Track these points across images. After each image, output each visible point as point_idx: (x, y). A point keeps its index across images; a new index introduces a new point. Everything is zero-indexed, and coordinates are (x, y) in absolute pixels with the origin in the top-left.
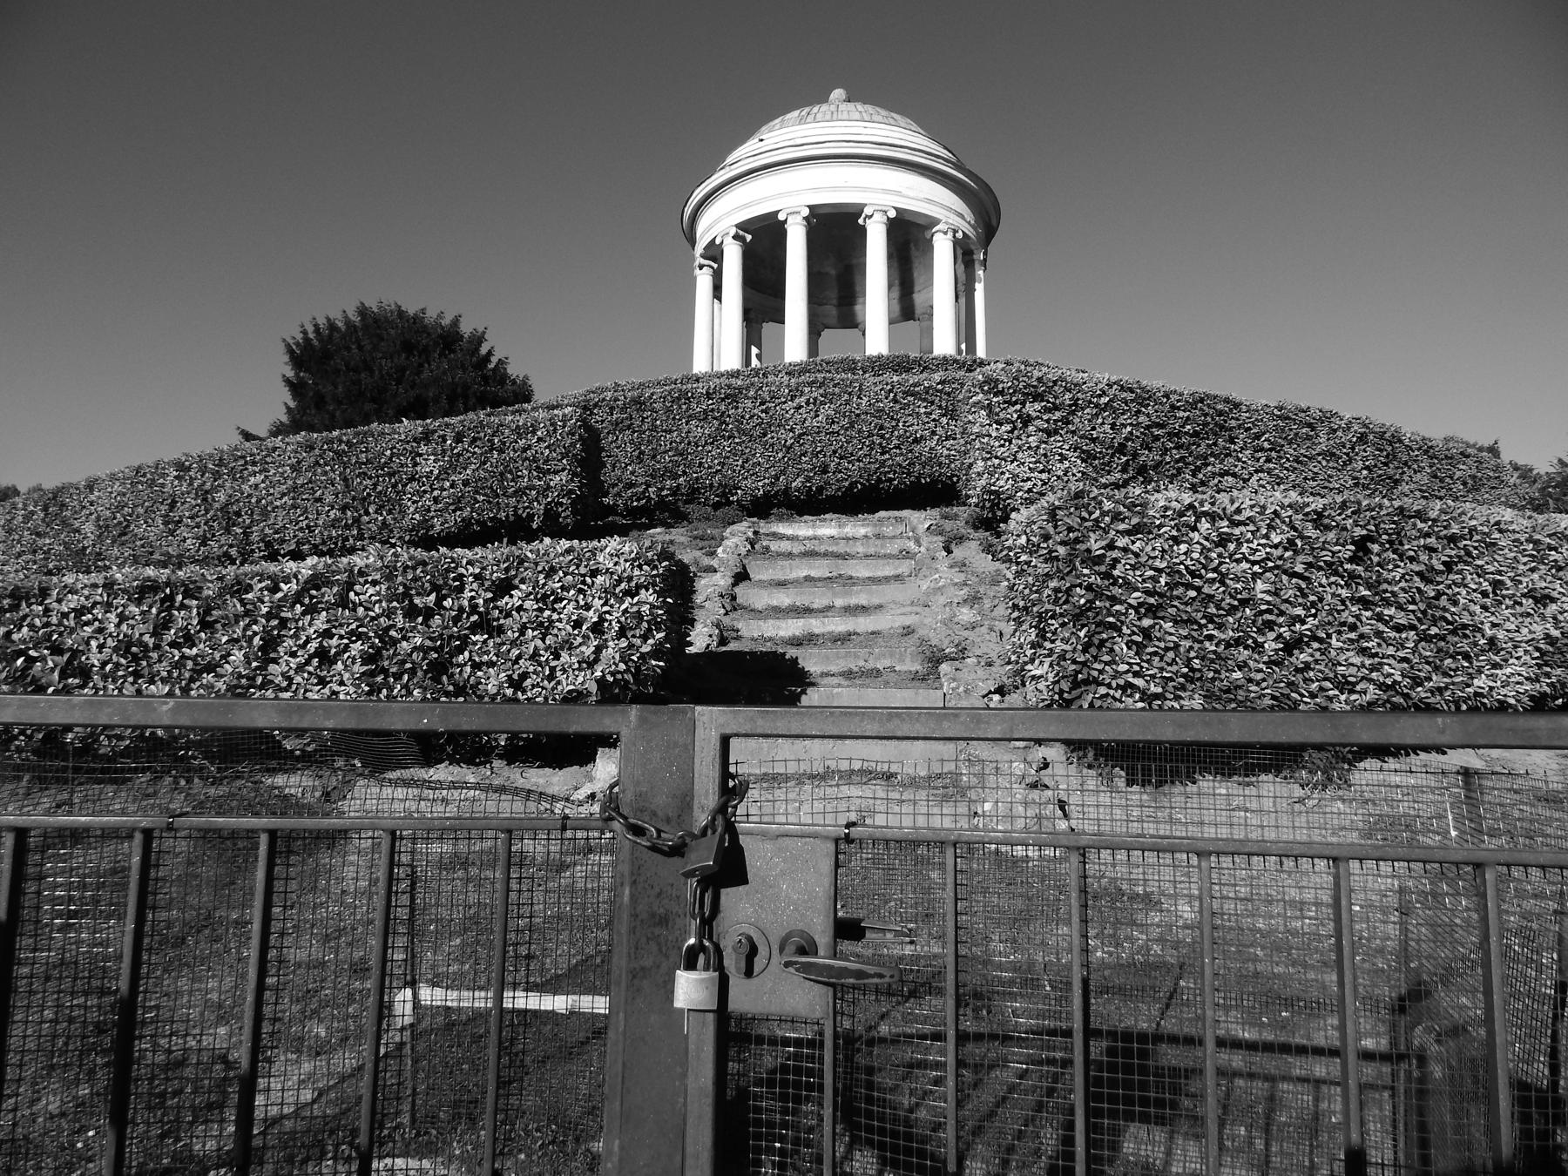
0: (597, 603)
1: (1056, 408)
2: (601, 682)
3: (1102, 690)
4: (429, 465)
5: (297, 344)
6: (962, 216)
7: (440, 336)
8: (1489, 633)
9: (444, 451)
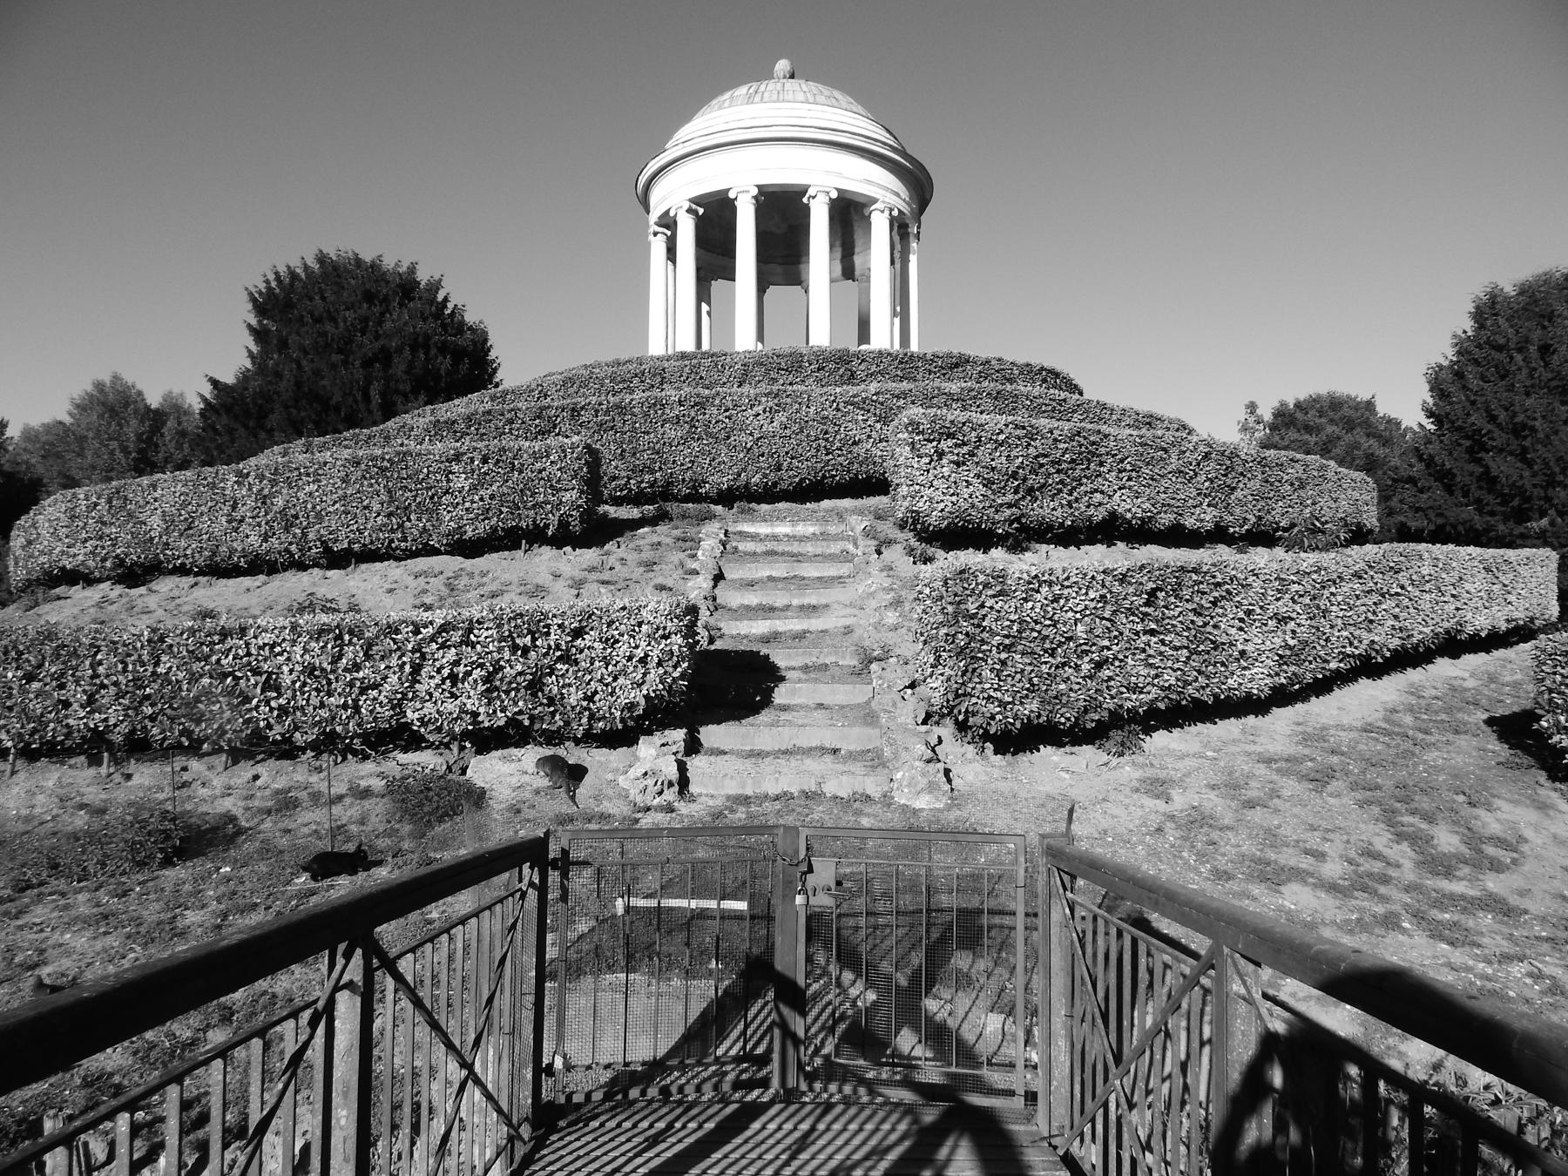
0: (643, 644)
1: (964, 444)
2: (647, 697)
3: (974, 700)
4: (461, 482)
5: (260, 293)
6: (898, 195)
7: (399, 286)
8: (1240, 647)
9: (473, 471)
